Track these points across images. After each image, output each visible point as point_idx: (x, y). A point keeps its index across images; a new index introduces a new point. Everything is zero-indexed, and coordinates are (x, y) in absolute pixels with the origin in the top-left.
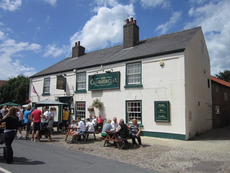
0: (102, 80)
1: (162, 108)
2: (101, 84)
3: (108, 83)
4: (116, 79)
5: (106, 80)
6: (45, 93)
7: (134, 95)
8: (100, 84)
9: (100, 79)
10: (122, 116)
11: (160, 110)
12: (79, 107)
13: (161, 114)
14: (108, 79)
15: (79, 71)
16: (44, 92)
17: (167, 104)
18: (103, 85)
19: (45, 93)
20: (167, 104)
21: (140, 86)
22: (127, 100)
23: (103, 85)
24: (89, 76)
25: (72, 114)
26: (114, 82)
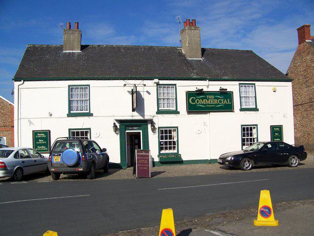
0: (210, 100)
1: (41, 138)
2: (209, 104)
3: (219, 104)
4: (229, 100)
5: (215, 100)
6: (71, 112)
7: (249, 119)
8: (206, 105)
9: (206, 98)
10: (268, 139)
11: (276, 134)
12: (250, 138)
13: (40, 145)
14: (218, 99)
15: (161, 82)
16: (69, 112)
17: (280, 127)
18: (211, 106)
19: (71, 112)
20: (280, 127)
21: (90, 115)
22: (242, 124)
23: (211, 106)
24: (189, 94)
25: (85, 149)
26: (227, 103)
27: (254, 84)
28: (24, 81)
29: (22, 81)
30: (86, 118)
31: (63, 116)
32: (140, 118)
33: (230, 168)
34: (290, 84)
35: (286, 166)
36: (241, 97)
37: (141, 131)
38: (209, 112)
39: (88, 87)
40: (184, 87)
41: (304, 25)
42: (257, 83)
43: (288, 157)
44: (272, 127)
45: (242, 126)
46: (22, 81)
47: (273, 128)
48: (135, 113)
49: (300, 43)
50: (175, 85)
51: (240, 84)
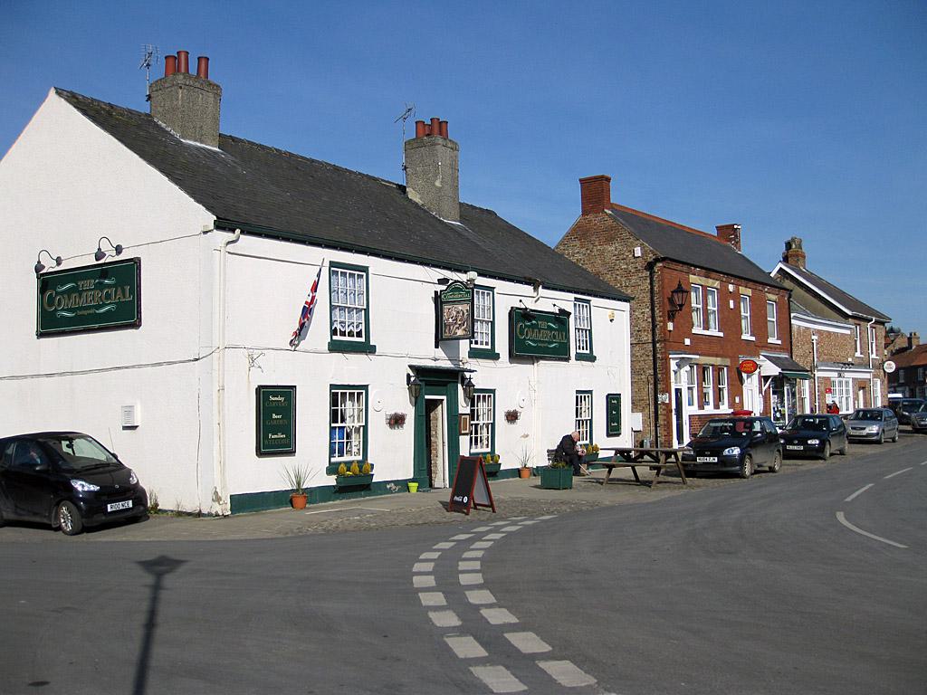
11: (274, 416)
17: (288, 392)
18: (85, 312)
20: (288, 392)
21: (367, 349)
27: (588, 301)
28: (242, 232)
29: (238, 231)
30: (362, 357)
31: (319, 349)
32: (447, 364)
33: (546, 486)
34: (626, 306)
35: (47, 527)
36: (332, 308)
37: (444, 397)
38: (538, 359)
39: (364, 274)
40: (509, 296)
41: (602, 177)
42: (595, 301)
43: (81, 499)
44: (263, 393)
45: (332, 387)
46: (238, 231)
47: (266, 395)
48: (440, 353)
49: (585, 213)
50: (365, 269)
51: (576, 299)
